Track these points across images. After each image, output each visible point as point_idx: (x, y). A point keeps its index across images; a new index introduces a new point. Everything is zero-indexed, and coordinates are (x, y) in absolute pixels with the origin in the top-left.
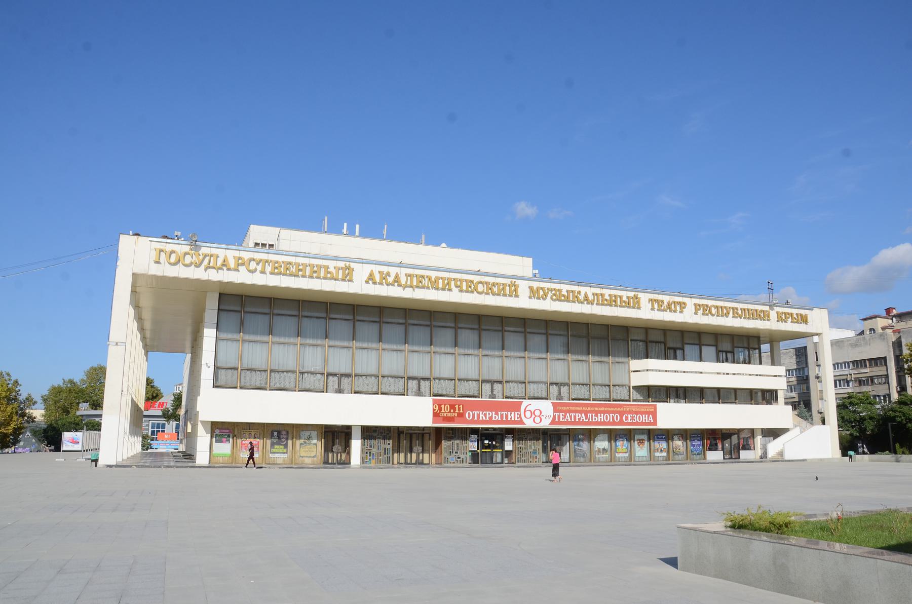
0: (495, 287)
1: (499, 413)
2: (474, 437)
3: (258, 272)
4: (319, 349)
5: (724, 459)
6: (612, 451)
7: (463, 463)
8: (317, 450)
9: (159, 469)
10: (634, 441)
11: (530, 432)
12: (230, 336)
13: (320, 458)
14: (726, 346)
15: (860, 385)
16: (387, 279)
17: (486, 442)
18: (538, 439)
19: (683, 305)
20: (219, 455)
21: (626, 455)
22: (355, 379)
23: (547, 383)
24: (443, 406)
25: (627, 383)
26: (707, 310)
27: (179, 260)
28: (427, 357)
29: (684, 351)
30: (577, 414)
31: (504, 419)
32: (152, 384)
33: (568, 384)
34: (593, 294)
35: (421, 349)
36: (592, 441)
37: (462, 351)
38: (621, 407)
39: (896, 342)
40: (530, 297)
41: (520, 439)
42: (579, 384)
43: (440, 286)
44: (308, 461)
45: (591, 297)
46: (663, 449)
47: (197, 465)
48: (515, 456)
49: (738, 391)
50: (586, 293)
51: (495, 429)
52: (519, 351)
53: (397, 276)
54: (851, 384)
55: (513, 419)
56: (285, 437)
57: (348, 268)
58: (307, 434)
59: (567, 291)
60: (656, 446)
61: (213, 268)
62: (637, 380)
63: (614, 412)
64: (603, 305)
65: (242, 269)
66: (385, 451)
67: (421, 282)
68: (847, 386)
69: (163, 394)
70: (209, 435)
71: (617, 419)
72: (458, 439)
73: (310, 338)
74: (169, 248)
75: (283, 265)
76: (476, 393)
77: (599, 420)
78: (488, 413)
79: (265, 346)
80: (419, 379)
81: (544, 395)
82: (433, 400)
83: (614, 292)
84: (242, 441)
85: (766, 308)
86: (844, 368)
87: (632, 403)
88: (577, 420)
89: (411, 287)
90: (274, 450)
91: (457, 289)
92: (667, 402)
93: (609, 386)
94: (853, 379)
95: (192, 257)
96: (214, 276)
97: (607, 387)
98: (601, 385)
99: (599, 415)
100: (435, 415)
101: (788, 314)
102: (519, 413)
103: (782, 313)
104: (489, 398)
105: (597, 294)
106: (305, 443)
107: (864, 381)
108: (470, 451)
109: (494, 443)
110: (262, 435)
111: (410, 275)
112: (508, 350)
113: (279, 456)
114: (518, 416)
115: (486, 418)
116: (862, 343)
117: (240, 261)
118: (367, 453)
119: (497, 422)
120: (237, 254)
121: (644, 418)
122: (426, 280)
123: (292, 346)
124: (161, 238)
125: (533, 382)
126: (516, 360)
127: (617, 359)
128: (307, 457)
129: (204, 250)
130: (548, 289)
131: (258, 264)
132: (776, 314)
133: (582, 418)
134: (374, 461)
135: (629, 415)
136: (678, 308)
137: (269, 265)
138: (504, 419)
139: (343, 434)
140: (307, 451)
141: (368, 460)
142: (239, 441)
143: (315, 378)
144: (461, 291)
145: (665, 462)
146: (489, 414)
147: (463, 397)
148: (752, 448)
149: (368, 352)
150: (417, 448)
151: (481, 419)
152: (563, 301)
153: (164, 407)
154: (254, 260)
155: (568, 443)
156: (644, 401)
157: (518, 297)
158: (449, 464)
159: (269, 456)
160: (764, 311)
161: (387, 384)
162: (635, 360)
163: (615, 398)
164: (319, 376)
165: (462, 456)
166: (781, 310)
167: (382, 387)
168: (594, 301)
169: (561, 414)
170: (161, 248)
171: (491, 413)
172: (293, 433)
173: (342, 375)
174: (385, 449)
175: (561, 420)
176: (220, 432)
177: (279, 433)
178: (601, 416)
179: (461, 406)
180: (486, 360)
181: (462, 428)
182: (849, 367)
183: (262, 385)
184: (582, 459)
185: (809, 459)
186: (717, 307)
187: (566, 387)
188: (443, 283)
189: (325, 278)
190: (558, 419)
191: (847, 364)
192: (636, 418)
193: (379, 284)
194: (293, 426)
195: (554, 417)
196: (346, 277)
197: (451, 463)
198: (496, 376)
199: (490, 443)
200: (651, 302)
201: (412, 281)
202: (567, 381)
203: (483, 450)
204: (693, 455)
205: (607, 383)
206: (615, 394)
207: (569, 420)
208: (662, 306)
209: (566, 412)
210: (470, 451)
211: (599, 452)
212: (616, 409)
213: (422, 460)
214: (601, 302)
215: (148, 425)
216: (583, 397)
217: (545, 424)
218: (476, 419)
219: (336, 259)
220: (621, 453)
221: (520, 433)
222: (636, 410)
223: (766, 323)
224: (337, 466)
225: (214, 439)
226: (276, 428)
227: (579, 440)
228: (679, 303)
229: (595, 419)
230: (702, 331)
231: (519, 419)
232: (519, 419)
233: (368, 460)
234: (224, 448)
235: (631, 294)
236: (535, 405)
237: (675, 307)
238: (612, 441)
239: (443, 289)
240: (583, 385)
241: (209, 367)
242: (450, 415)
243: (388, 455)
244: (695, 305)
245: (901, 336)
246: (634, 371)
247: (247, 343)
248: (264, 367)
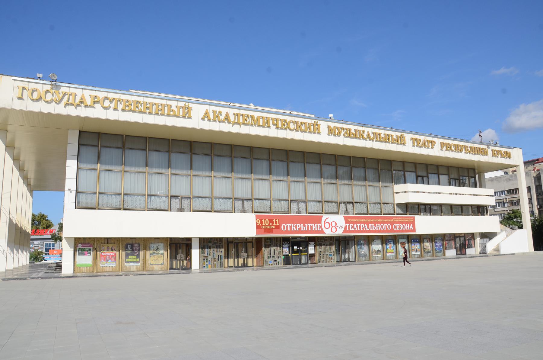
0: (303, 126)
1: (306, 225)
2: (286, 245)
3: (111, 109)
4: (163, 176)
5: (457, 255)
6: (384, 251)
7: (278, 265)
8: (164, 260)
9: (25, 280)
10: (398, 244)
11: (327, 239)
12: (89, 166)
13: (166, 265)
14: (454, 175)
15: (512, 205)
16: (219, 117)
17: (295, 248)
18: (332, 245)
19: (433, 143)
20: (81, 266)
21: (394, 254)
22: (193, 200)
23: (338, 202)
24: (264, 220)
26: (448, 147)
28: (249, 183)
29: (428, 178)
30: (362, 225)
31: (310, 230)
32: (46, 219)
33: (352, 203)
34: (373, 133)
35: (244, 176)
36: (370, 245)
37: (275, 178)
38: (391, 219)
39: (536, 177)
40: (329, 134)
41: (320, 245)
42: (360, 203)
43: (261, 123)
44: (156, 267)
45: (372, 136)
46: (417, 250)
47: (62, 276)
48: (317, 258)
49: (463, 206)
50: (368, 132)
51: (300, 237)
52: (316, 177)
53: (227, 115)
54: (506, 205)
55: (316, 230)
56: (138, 248)
58: (156, 245)
59: (355, 130)
60: (413, 247)
61: (73, 105)
62: (400, 199)
63: (387, 223)
64: (380, 141)
65: (97, 106)
66: (219, 258)
67: (246, 120)
68: (498, 207)
69: (54, 225)
70: (73, 249)
71: (389, 228)
72: (275, 246)
73: (155, 167)
74: (31, 86)
75: (133, 104)
76: (286, 210)
77: (377, 229)
78: (298, 225)
79: (119, 174)
80: (243, 200)
81: (336, 211)
82: (256, 215)
83: (387, 132)
84: (101, 253)
85: (485, 147)
86: (501, 194)
88: (362, 229)
89: (239, 124)
91: (274, 127)
92: (419, 215)
93: (380, 204)
94: (508, 202)
95: (53, 95)
96: (72, 111)
97: (378, 204)
98: (375, 203)
99: (377, 225)
100: (258, 227)
101: (499, 151)
102: (320, 225)
103: (495, 151)
104: (297, 214)
107: (515, 203)
108: (283, 255)
109: (301, 248)
110: (118, 247)
111: (237, 115)
112: (309, 177)
113: (133, 264)
114: (320, 227)
115: (296, 229)
116: (514, 178)
117: (96, 100)
118: (204, 259)
119: (305, 232)
120: (93, 93)
121: (407, 227)
122: (250, 118)
123: (141, 174)
125: (328, 202)
126: (314, 185)
127: (385, 184)
128: (156, 264)
130: (341, 128)
131: (111, 102)
132: (491, 151)
133: (365, 228)
134: (210, 266)
135: (397, 225)
137: (121, 103)
138: (310, 230)
139: (185, 245)
140: (156, 260)
141: (205, 266)
142: (99, 253)
143: (161, 200)
144: (277, 128)
145: (394, 260)
146: (299, 226)
148: (473, 247)
149: (203, 178)
150: (244, 255)
151: (293, 230)
152: (353, 138)
153: (54, 232)
154: (108, 99)
155: (354, 247)
156: (403, 215)
157: (320, 134)
158: (268, 266)
159: (124, 264)
160: (484, 149)
161: (218, 204)
162: (396, 184)
163: (385, 212)
164: (164, 198)
165: (278, 260)
167: (215, 207)
168: (374, 138)
169: (350, 225)
170: (24, 86)
172: (144, 245)
173: (183, 197)
174: (219, 255)
175: (351, 229)
176: (82, 246)
177: (132, 246)
178: (378, 226)
179: (278, 220)
180: (292, 185)
181: (277, 238)
182: (505, 194)
183: (117, 207)
184: (364, 259)
185: (517, 253)
186: (455, 145)
187: (351, 205)
188: (263, 121)
189: (169, 115)
190: (348, 229)
191: (503, 192)
192: (402, 227)
193: (213, 121)
194: (144, 239)
195: (346, 227)
196: (186, 115)
197: (269, 265)
199: (298, 248)
200: (412, 141)
201: (239, 119)
202: (351, 200)
203: (293, 254)
204: (437, 252)
205: (379, 201)
207: (356, 229)
208: (419, 143)
209: (353, 223)
210: (283, 255)
211: (375, 252)
212: (388, 221)
213: (247, 263)
214: (378, 139)
215: (43, 245)
217: (340, 233)
218: (289, 230)
220: (390, 253)
221: (319, 241)
222: (402, 221)
223: (485, 157)
224: (180, 271)
225: (77, 252)
227: (361, 244)
228: (431, 142)
229: (374, 228)
230: (439, 164)
231: (321, 230)
232: (321, 230)
233: (205, 266)
234: (86, 260)
235: (399, 134)
236: (332, 218)
237: (428, 144)
238: (384, 244)
239: (263, 126)
240: (362, 203)
241: (71, 192)
242: (269, 227)
243: (221, 261)
244: (441, 143)
245: (540, 173)
247: (104, 172)
248: (118, 192)
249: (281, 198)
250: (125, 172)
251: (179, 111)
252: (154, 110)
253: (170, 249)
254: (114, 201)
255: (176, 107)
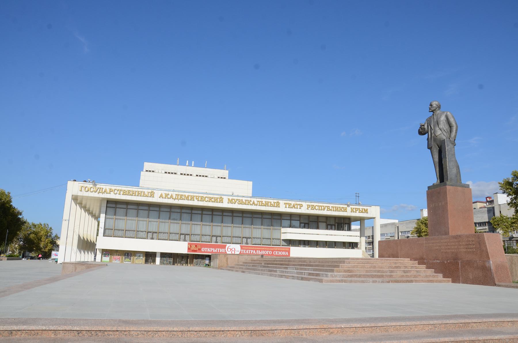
1: (216, 249)
3: (118, 194)
19: (301, 206)
25: (279, 238)
26: (313, 208)
27: (88, 190)
31: (218, 251)
33: (251, 238)
38: (272, 248)
40: (228, 203)
45: (256, 203)
52: (239, 224)
53: (254, 202)
55: (222, 252)
56: (130, 255)
57: (221, 198)
58: (139, 254)
62: (284, 237)
63: (269, 250)
65: (358, 212)
70: (101, 254)
72: (200, 259)
74: (85, 185)
78: (211, 249)
80: (185, 235)
83: (267, 200)
85: (346, 206)
87: (281, 247)
88: (251, 253)
90: (125, 260)
92: (299, 247)
99: (262, 251)
100: (189, 249)
103: (354, 208)
105: (333, 207)
106: (138, 258)
120: (110, 187)
121: (284, 253)
124: (83, 182)
129: (98, 186)
131: (118, 191)
135: (276, 252)
136: (299, 207)
138: (218, 251)
142: (112, 256)
144: (198, 201)
147: (204, 242)
151: (208, 251)
163: (263, 244)
164: (144, 232)
166: (353, 207)
169: (244, 250)
170: (82, 186)
171: (212, 249)
173: (154, 233)
177: (128, 254)
178: (263, 251)
179: (200, 246)
189: (270, 206)
195: (241, 251)
196: (192, 199)
198: (218, 234)
202: (251, 237)
205: (270, 238)
206: (273, 242)
207: (248, 253)
209: (246, 249)
216: (258, 243)
219: (148, 189)
225: (103, 255)
226: (126, 252)
229: (260, 253)
234: (106, 259)
235: (276, 201)
236: (232, 246)
237: (297, 206)
242: (195, 249)
246: (283, 233)
249: (207, 234)
250: (233, 227)
251: (246, 202)
252: (213, 200)
253: (145, 257)
254: (120, 233)
255: (274, 202)
